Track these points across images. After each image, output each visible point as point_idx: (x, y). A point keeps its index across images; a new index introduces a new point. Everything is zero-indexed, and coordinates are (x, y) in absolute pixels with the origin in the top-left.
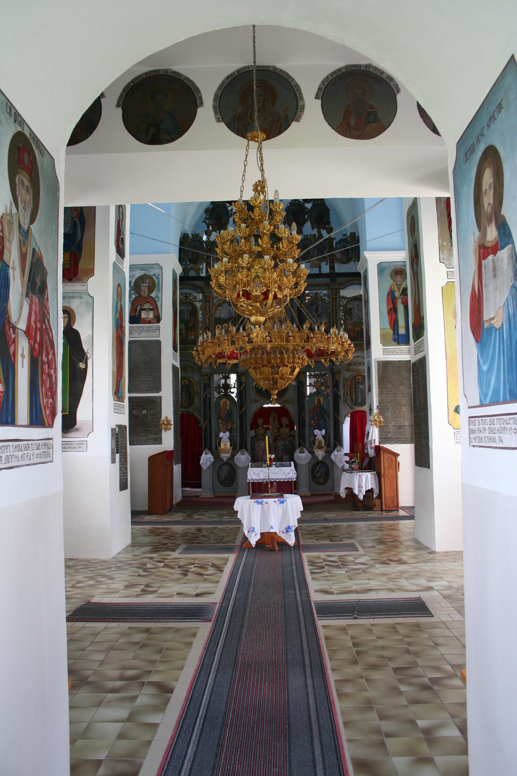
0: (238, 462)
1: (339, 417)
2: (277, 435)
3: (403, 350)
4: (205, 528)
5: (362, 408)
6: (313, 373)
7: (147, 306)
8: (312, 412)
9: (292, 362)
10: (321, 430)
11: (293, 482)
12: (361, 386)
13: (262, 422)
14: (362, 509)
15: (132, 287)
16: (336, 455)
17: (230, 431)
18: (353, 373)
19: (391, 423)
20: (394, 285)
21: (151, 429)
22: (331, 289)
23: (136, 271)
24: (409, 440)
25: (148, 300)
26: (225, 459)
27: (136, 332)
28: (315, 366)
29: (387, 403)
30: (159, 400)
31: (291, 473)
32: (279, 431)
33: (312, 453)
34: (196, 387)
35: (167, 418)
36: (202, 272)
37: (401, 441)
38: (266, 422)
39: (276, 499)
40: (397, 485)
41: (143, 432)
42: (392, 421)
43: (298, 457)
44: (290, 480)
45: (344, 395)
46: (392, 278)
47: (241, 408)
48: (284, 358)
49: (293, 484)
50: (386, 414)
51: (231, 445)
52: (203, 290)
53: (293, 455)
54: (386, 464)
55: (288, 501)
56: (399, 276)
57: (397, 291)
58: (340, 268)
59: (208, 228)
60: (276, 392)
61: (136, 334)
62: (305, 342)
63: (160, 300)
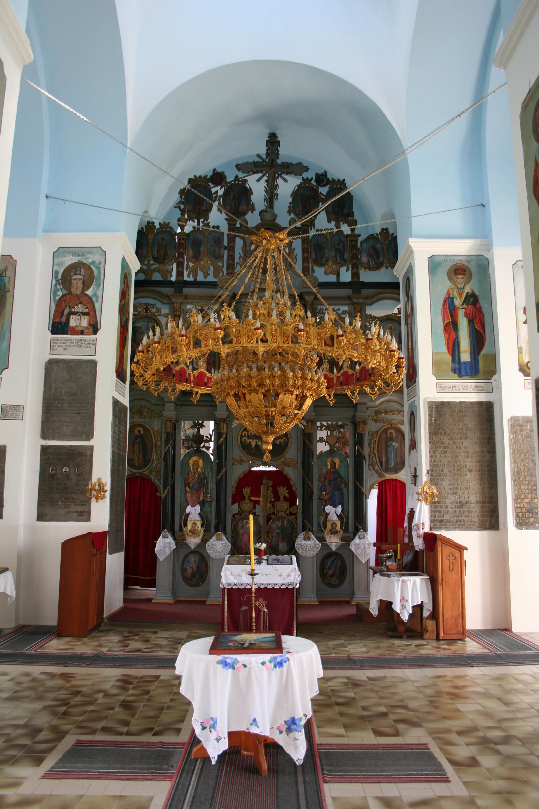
0: (212, 551)
1: (363, 487)
2: (271, 512)
3: (467, 386)
4: (136, 678)
5: (396, 475)
6: (325, 423)
7: (79, 308)
8: (323, 479)
9: (301, 386)
10: (335, 506)
11: (295, 590)
12: (394, 444)
13: (249, 493)
14: (405, 637)
15: (59, 280)
16: (358, 544)
17: (202, 504)
18: (383, 424)
19: (449, 498)
20: (452, 289)
21: (75, 496)
22: (354, 304)
23: (65, 256)
24: (477, 524)
25: (82, 299)
26: (193, 546)
27: (60, 346)
28: (334, 403)
29: (443, 466)
30: (88, 453)
31: (293, 575)
32: (273, 506)
33: (322, 539)
34: (155, 438)
35: (99, 480)
36: (171, 276)
37: (464, 527)
38: (256, 492)
39: (267, 657)
40: (463, 599)
41: (62, 502)
42: (451, 494)
43: (301, 546)
44: (290, 587)
45: (369, 456)
46: (450, 278)
47: (219, 471)
48: (288, 378)
49: (295, 592)
50: (441, 484)
51: (202, 526)
52: (171, 299)
53: (294, 543)
54: (446, 563)
55: (291, 661)
56: (460, 276)
57: (458, 298)
58: (366, 276)
59: (183, 214)
60: (272, 438)
61: (60, 350)
62: (326, 345)
63: (100, 300)
